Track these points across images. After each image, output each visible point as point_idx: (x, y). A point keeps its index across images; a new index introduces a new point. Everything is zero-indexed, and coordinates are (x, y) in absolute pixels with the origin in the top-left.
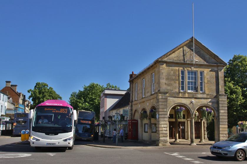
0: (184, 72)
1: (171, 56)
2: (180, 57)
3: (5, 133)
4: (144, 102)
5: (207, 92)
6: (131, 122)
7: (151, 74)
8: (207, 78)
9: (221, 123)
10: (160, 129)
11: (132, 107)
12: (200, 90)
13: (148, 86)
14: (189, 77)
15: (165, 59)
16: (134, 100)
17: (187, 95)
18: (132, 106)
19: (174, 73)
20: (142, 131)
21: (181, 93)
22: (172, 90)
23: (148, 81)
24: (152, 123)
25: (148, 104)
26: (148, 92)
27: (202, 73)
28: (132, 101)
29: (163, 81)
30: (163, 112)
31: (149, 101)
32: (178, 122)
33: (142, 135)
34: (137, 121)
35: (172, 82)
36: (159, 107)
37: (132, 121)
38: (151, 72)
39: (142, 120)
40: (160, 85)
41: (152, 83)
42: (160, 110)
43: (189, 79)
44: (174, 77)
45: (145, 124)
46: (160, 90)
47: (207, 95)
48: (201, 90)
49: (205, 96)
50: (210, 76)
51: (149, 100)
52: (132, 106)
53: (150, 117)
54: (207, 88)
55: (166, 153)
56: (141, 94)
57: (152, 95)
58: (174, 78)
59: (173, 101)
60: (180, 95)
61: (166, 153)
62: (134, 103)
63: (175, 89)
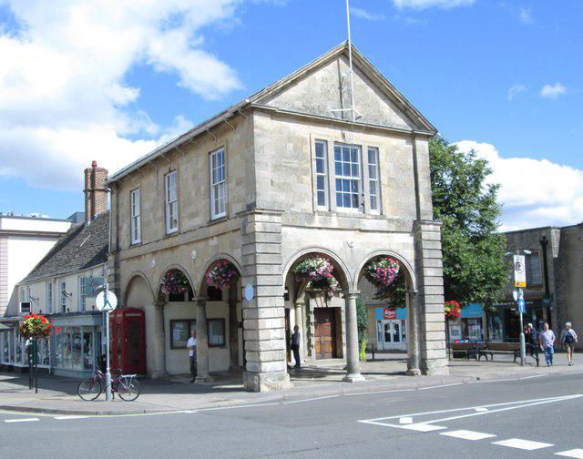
0: (325, 146)
1: (286, 94)
2: (311, 98)
3: (3, 323)
4: (139, 257)
5: (388, 214)
6: (125, 318)
7: (210, 153)
8: (388, 171)
9: (428, 308)
10: (262, 335)
11: (119, 267)
12: (369, 205)
13: (193, 194)
14: (338, 167)
15: (271, 104)
16: (124, 244)
17: (334, 222)
18: (117, 265)
19: (295, 148)
20: (164, 346)
21: (320, 213)
22: (292, 206)
23: (194, 177)
24: (208, 317)
25: (194, 253)
26: (193, 215)
27: (373, 152)
28: (118, 250)
29: (266, 172)
30: (267, 278)
31: (201, 245)
32: (510, 291)
33: (164, 356)
34: (142, 312)
35: (292, 179)
36: (255, 260)
37: (124, 313)
38: (164, 170)
39: (163, 309)
40: (257, 186)
41: (212, 184)
42: (260, 270)
43: (338, 171)
44: (297, 161)
45: (173, 322)
46: (254, 204)
47: (390, 221)
48: (373, 207)
49: (383, 225)
50: (395, 166)
51: (200, 240)
52: (117, 265)
53: (203, 298)
54: (387, 201)
55: (366, 421)
56: (161, 224)
57: (212, 223)
58: (295, 164)
59: (296, 242)
60: (317, 222)
61: (366, 421)
62: (123, 255)
63: (301, 200)
